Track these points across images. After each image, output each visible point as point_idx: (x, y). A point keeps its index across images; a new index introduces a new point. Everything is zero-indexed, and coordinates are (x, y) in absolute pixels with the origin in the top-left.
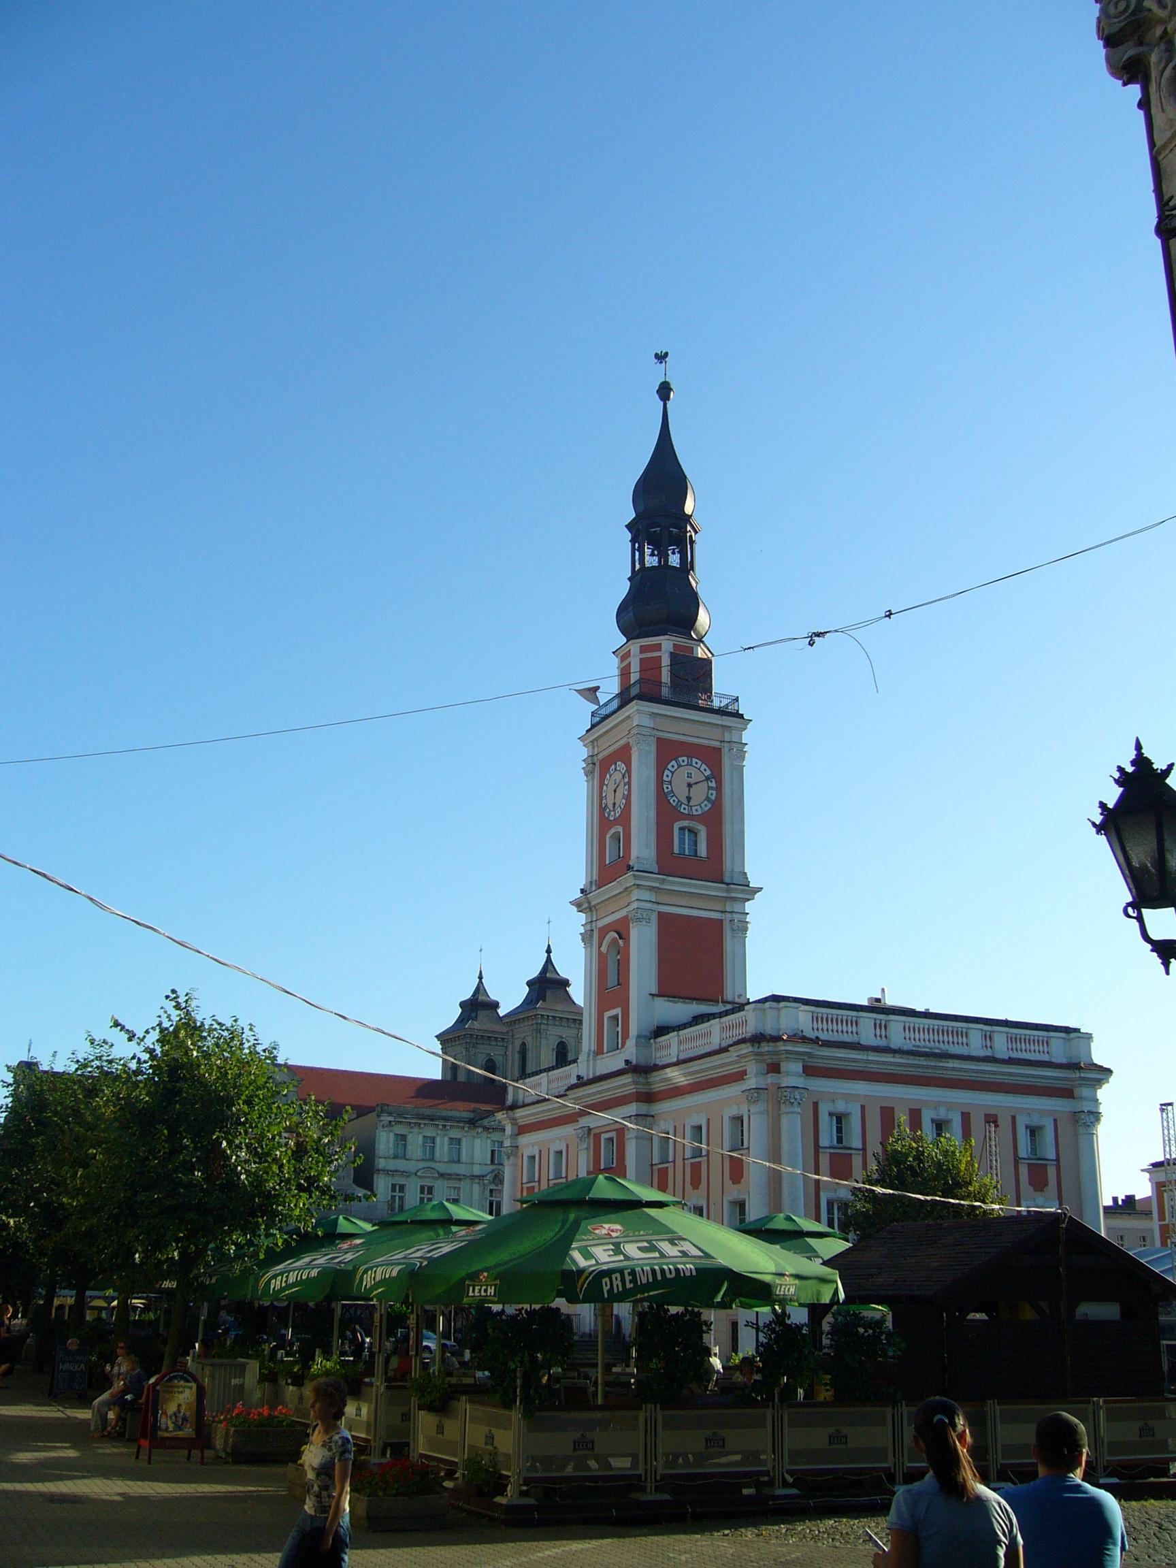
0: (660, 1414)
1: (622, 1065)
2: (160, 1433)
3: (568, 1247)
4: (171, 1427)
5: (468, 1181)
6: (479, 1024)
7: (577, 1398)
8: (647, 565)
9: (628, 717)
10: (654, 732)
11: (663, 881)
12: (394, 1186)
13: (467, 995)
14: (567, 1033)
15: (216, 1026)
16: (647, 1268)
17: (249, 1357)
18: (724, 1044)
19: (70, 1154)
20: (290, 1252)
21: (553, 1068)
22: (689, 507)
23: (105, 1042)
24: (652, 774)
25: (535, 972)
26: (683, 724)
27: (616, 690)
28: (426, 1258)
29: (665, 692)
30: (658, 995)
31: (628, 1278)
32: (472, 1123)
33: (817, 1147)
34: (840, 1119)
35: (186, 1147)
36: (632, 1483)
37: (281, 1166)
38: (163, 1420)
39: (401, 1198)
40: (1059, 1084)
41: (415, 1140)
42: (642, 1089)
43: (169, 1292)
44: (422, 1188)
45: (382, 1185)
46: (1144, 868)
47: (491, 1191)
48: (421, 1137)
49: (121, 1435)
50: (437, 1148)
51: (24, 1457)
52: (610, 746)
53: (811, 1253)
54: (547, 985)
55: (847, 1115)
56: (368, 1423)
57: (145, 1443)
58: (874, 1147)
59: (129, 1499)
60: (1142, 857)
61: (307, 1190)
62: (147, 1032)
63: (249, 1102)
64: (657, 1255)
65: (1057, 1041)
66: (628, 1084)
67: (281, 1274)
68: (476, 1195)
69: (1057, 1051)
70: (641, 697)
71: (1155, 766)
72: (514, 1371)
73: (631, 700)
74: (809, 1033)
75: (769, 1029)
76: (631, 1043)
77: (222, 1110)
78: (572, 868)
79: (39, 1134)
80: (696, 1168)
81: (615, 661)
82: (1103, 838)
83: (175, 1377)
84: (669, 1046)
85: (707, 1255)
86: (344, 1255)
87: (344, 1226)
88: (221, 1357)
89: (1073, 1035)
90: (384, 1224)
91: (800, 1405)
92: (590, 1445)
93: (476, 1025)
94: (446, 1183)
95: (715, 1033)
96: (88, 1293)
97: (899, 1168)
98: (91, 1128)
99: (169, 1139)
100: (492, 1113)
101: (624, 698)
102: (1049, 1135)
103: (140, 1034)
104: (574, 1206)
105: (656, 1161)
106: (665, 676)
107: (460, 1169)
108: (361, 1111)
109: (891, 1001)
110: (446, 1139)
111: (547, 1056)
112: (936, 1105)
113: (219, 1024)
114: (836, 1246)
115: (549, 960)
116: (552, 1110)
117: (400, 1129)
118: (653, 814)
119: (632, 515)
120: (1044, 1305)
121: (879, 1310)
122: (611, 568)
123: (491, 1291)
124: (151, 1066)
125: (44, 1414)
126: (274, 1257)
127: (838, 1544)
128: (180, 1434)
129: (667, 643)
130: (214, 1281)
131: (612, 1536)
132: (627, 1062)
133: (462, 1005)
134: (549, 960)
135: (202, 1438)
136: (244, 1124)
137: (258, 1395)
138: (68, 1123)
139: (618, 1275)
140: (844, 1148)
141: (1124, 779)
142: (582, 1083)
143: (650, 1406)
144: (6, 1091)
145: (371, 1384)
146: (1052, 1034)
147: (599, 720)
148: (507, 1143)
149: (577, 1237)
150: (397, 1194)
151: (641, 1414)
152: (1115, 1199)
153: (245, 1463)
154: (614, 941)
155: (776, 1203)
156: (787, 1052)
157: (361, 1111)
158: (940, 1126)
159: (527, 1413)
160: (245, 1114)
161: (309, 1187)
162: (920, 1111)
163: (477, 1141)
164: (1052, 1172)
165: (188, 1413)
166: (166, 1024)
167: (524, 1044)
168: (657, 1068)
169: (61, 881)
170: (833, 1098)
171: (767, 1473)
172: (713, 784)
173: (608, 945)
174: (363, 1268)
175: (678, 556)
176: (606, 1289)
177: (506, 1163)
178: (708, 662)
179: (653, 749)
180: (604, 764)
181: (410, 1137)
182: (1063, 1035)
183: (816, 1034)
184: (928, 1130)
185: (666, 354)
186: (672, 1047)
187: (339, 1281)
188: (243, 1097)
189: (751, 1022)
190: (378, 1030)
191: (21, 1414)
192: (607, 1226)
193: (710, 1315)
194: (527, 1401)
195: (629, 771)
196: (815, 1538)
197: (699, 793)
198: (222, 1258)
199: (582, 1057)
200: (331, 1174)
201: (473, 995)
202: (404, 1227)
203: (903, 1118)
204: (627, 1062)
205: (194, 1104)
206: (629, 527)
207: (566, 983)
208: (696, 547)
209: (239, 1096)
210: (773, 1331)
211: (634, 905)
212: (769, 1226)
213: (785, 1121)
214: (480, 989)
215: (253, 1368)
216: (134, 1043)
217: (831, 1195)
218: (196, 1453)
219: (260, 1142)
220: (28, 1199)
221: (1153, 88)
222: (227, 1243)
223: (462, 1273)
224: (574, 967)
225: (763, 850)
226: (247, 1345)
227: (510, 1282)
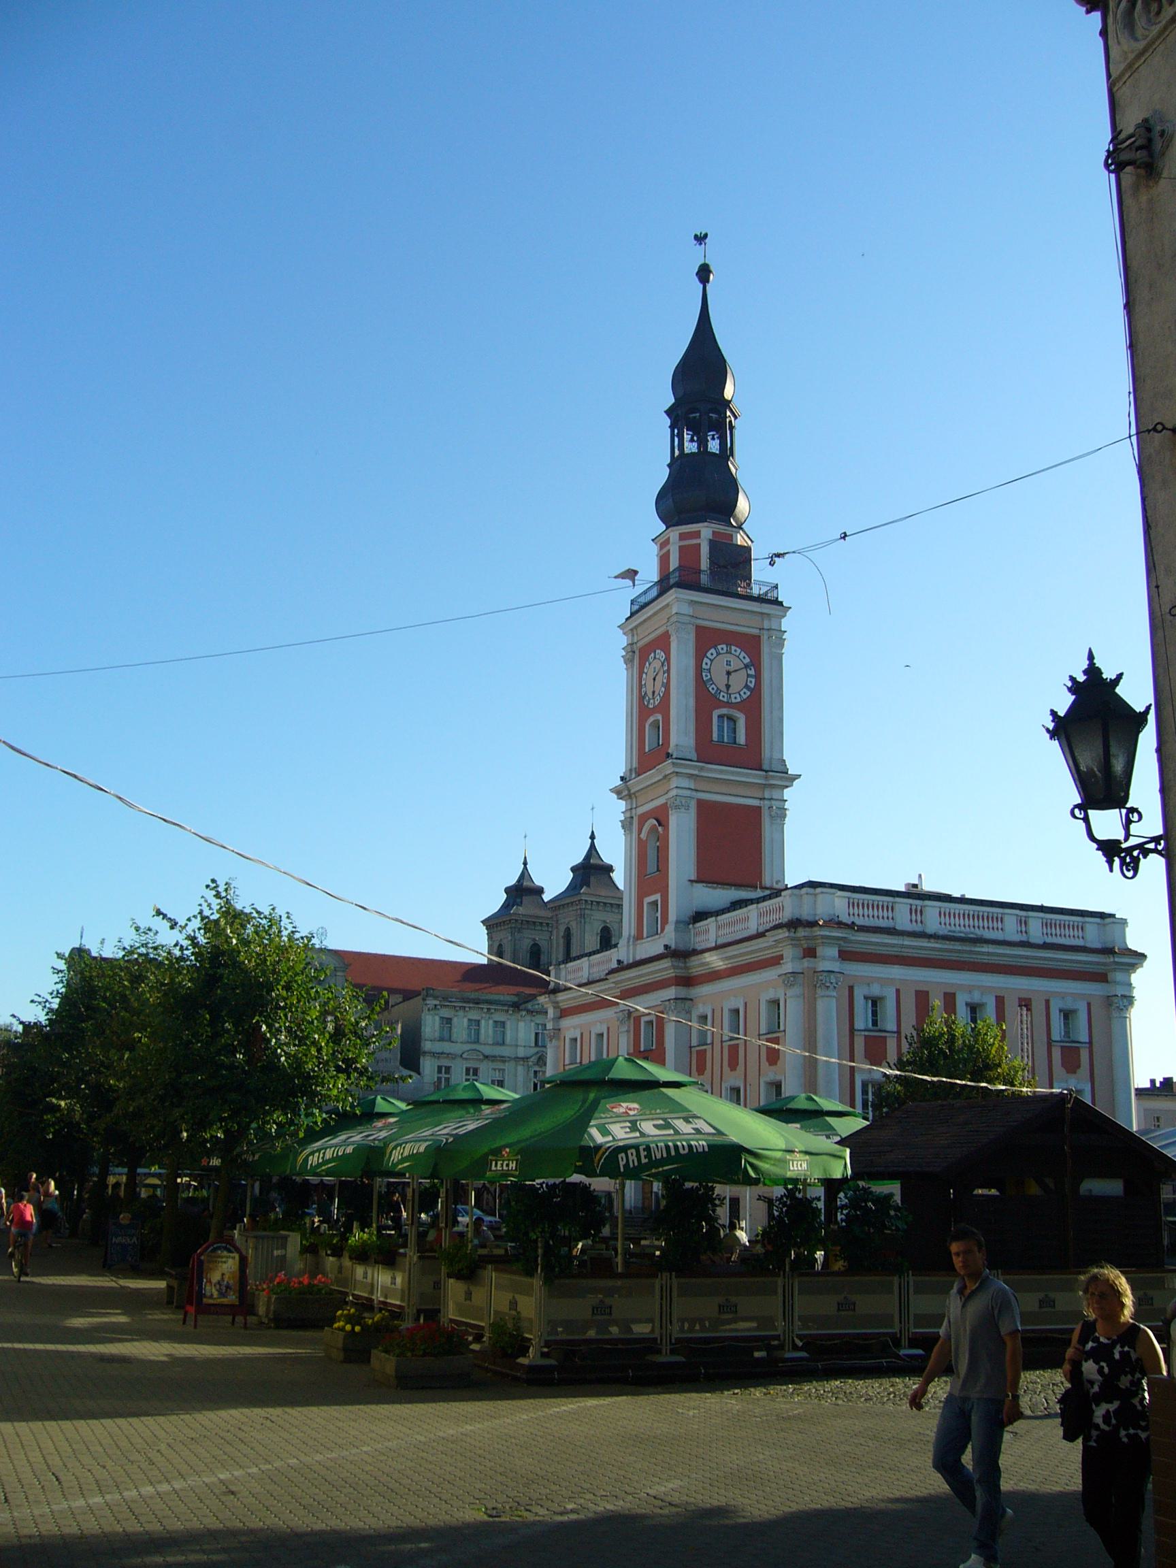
0: (675, 1281)
1: (661, 950)
2: (205, 1300)
3: (587, 1125)
4: (215, 1294)
5: (512, 1064)
6: (524, 909)
7: (599, 1266)
8: (687, 451)
9: (667, 605)
10: (693, 620)
11: (702, 769)
12: (440, 1068)
13: (512, 881)
14: (610, 918)
15: (255, 915)
16: (661, 1144)
17: (293, 1231)
18: (761, 929)
19: (118, 1038)
20: (329, 1130)
21: (594, 953)
22: (728, 392)
23: (150, 930)
24: (692, 662)
25: (578, 858)
26: (723, 612)
27: (655, 577)
28: (451, 1135)
29: (704, 579)
30: (697, 882)
31: (643, 1154)
32: (516, 1006)
33: (852, 1030)
34: (875, 1002)
35: (228, 1031)
36: (649, 1345)
37: (319, 1050)
38: (208, 1288)
39: (447, 1080)
40: (1090, 968)
41: (461, 1023)
42: (680, 972)
43: (215, 1168)
44: (468, 1070)
45: (428, 1066)
46: (1091, 772)
47: (535, 1072)
48: (466, 1020)
49: (170, 1302)
50: (482, 1031)
51: (78, 1322)
52: (648, 635)
53: (829, 1131)
54: (591, 870)
55: (882, 998)
56: (403, 1291)
57: (191, 1310)
58: (908, 1029)
59: (175, 1361)
60: (1090, 763)
61: (347, 1072)
62: (189, 920)
63: (288, 987)
64: (672, 1132)
65: (1091, 927)
66: (666, 969)
67: (319, 1151)
68: (520, 1078)
69: (1092, 936)
70: (679, 585)
71: (1104, 676)
72: (536, 1241)
73: (671, 588)
74: (845, 919)
75: (806, 914)
76: (670, 928)
77: (261, 996)
78: (614, 758)
79: (89, 1018)
80: (734, 1050)
81: (655, 549)
82: (1055, 744)
83: (219, 1248)
84: (707, 931)
85: (720, 1133)
86: (378, 1132)
87: (381, 1105)
88: (265, 1230)
89: (1108, 920)
90: (418, 1104)
91: (818, 1274)
92: (607, 1311)
93: (521, 910)
94: (491, 1065)
95: (752, 919)
96: (140, 1170)
97: (932, 1052)
98: (138, 1013)
99: (212, 1023)
100: (534, 997)
101: (664, 585)
102: (890, 1007)
103: (182, 922)
104: (596, 1085)
105: (694, 1043)
106: (705, 564)
107: (505, 1051)
108: (408, 995)
109: (928, 886)
110: (491, 1022)
111: (591, 940)
112: (970, 989)
113: (258, 912)
114: (855, 1124)
115: (593, 846)
116: (574, 998)
117: (446, 1013)
118: (692, 702)
119: (671, 400)
120: (1050, 1182)
121: (893, 1188)
122: (651, 455)
123: (513, 1165)
124: (193, 954)
125: (99, 1284)
126: (313, 1135)
127: (840, 1402)
128: (225, 1301)
129: (706, 531)
130: (256, 1157)
131: (626, 1394)
132: (666, 947)
133: (507, 890)
134: (593, 846)
135: (245, 1306)
136: (284, 1008)
137: (299, 1266)
138: (115, 1008)
139: (633, 1151)
140: (880, 1031)
141: (1075, 687)
142: (622, 967)
143: (666, 1275)
144: (56, 978)
145: (405, 1255)
146: (1088, 919)
147: (638, 607)
148: (550, 1026)
149: (596, 1115)
150: (444, 1075)
151: (657, 1282)
152: (1153, 1082)
153: (287, 1328)
154: (653, 829)
155: (811, 1085)
156: (823, 937)
157: (408, 995)
158: (974, 1009)
159: (548, 1280)
160: (285, 999)
161: (348, 1067)
162: (954, 995)
163: (521, 1024)
164: (1084, 1055)
165: (231, 1282)
166: (207, 912)
167: (568, 930)
168: (696, 952)
169: (91, 782)
170: (869, 982)
171: (777, 1337)
172: (752, 672)
173: (648, 830)
174: (392, 1145)
175: (717, 441)
176: (622, 1164)
177: (549, 1045)
178: (748, 549)
179: (692, 636)
180: (644, 652)
181: (455, 1020)
182: (1098, 920)
183: (852, 919)
184: (962, 1013)
185: (706, 236)
186: (710, 931)
187: (372, 1156)
188: (282, 983)
189: (787, 908)
190: (397, 920)
191: (75, 1283)
192: (624, 1105)
193: (719, 1189)
194: (548, 1268)
195: (668, 659)
196: (820, 1397)
197: (738, 681)
198: (264, 1136)
199: (622, 942)
200: (368, 1055)
201: (518, 881)
202: (437, 1106)
203: (937, 1003)
204: (666, 947)
205: (234, 989)
206: (669, 412)
207: (610, 869)
208: (736, 432)
209: (278, 981)
210: (784, 1204)
211: (674, 793)
212: (789, 1106)
213: (821, 1005)
214: (525, 874)
215: (295, 1240)
216: (176, 931)
217: (866, 1077)
218: (240, 1319)
219: (299, 1026)
220: (80, 1081)
221: (1110, 20)
222: (268, 1122)
223: (486, 1150)
224: (616, 852)
225: (801, 737)
226: (293, 1219)
227: (531, 1157)
